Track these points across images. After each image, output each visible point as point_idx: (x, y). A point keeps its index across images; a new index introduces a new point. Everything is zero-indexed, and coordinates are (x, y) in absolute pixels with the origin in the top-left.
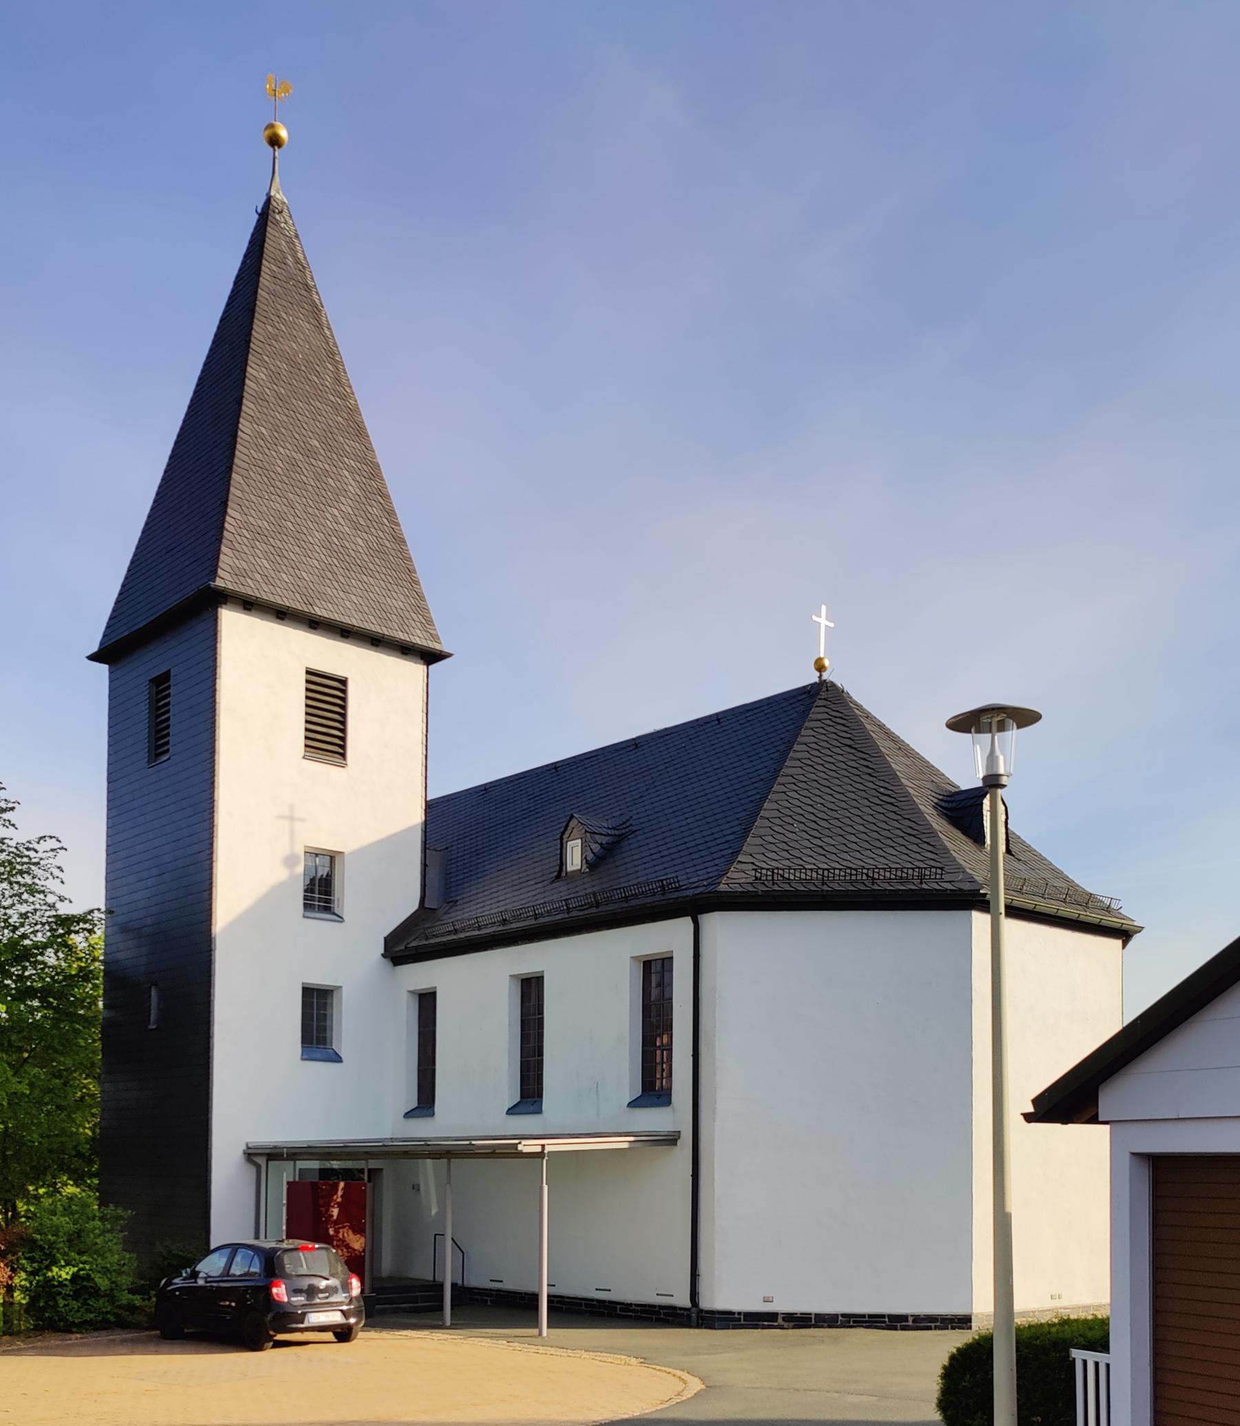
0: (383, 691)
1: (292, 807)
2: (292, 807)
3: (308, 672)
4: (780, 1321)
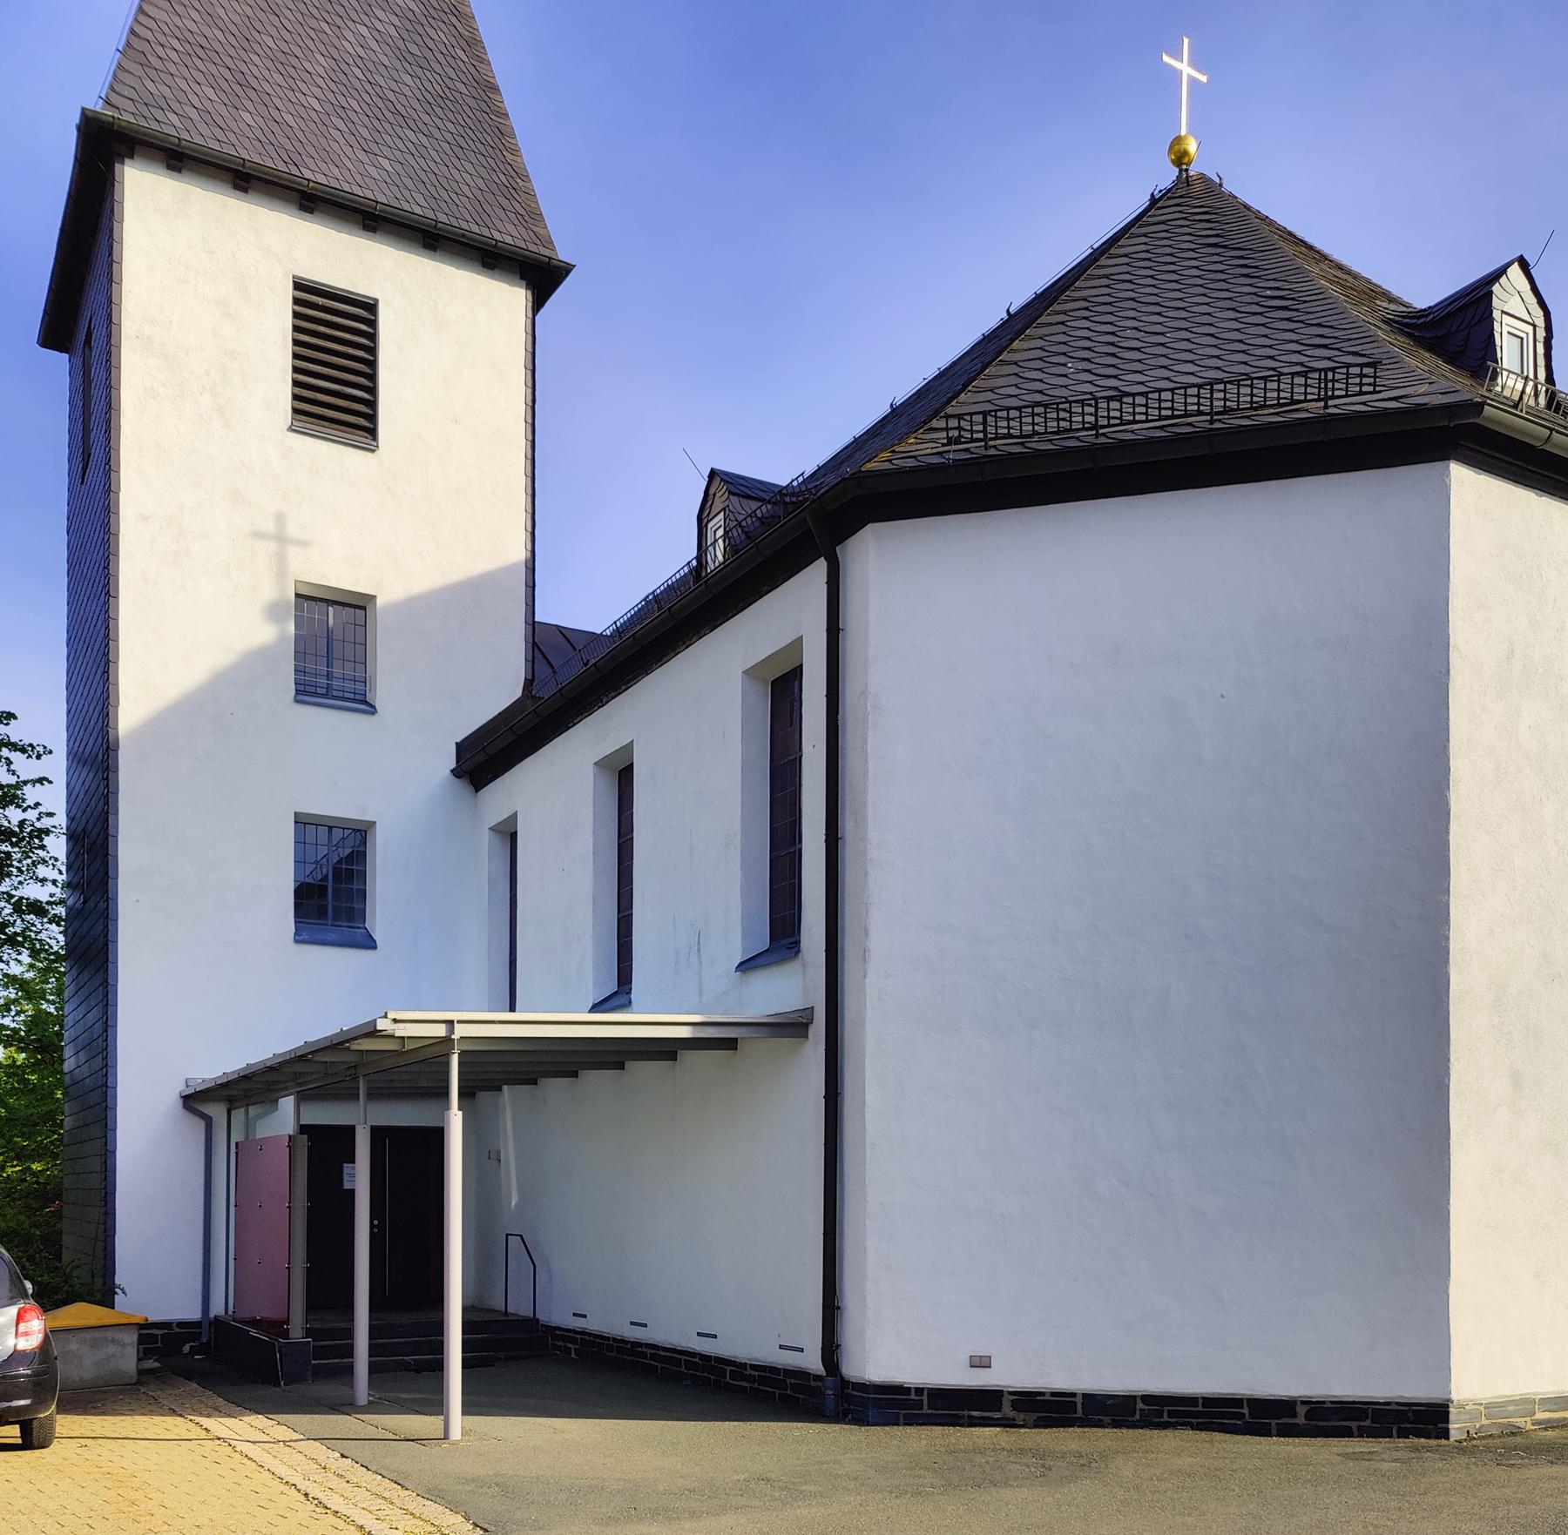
0: (446, 330)
1: (280, 518)
2: (280, 518)
3: (299, 285)
4: (1007, 1410)
